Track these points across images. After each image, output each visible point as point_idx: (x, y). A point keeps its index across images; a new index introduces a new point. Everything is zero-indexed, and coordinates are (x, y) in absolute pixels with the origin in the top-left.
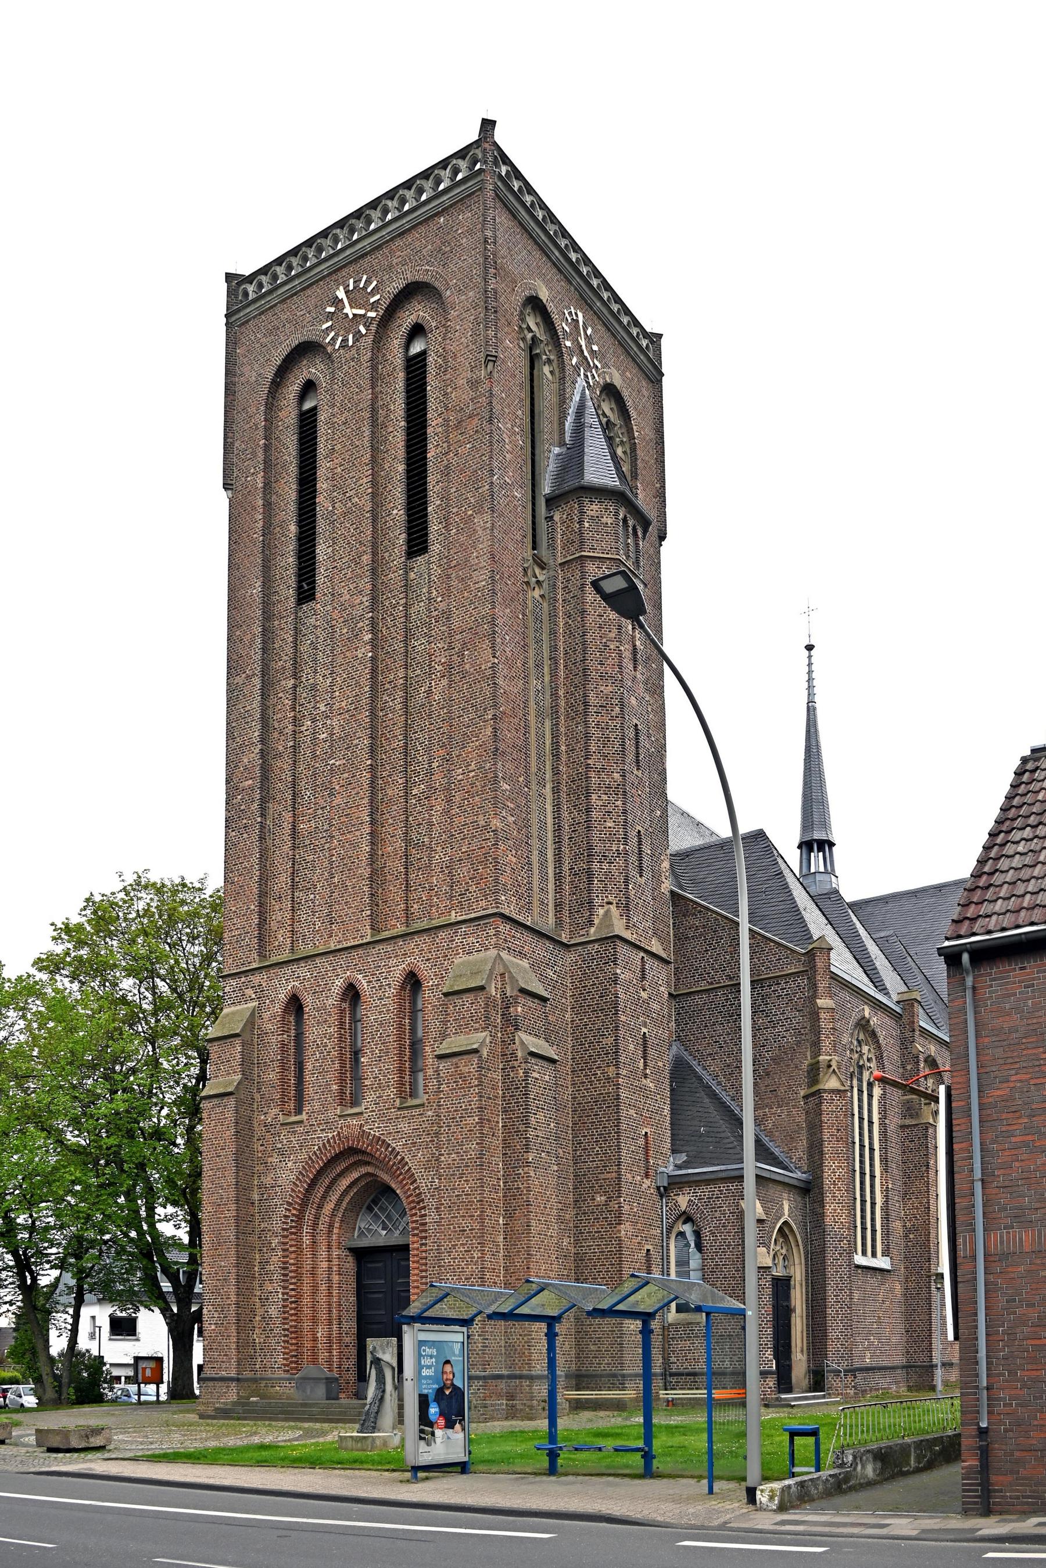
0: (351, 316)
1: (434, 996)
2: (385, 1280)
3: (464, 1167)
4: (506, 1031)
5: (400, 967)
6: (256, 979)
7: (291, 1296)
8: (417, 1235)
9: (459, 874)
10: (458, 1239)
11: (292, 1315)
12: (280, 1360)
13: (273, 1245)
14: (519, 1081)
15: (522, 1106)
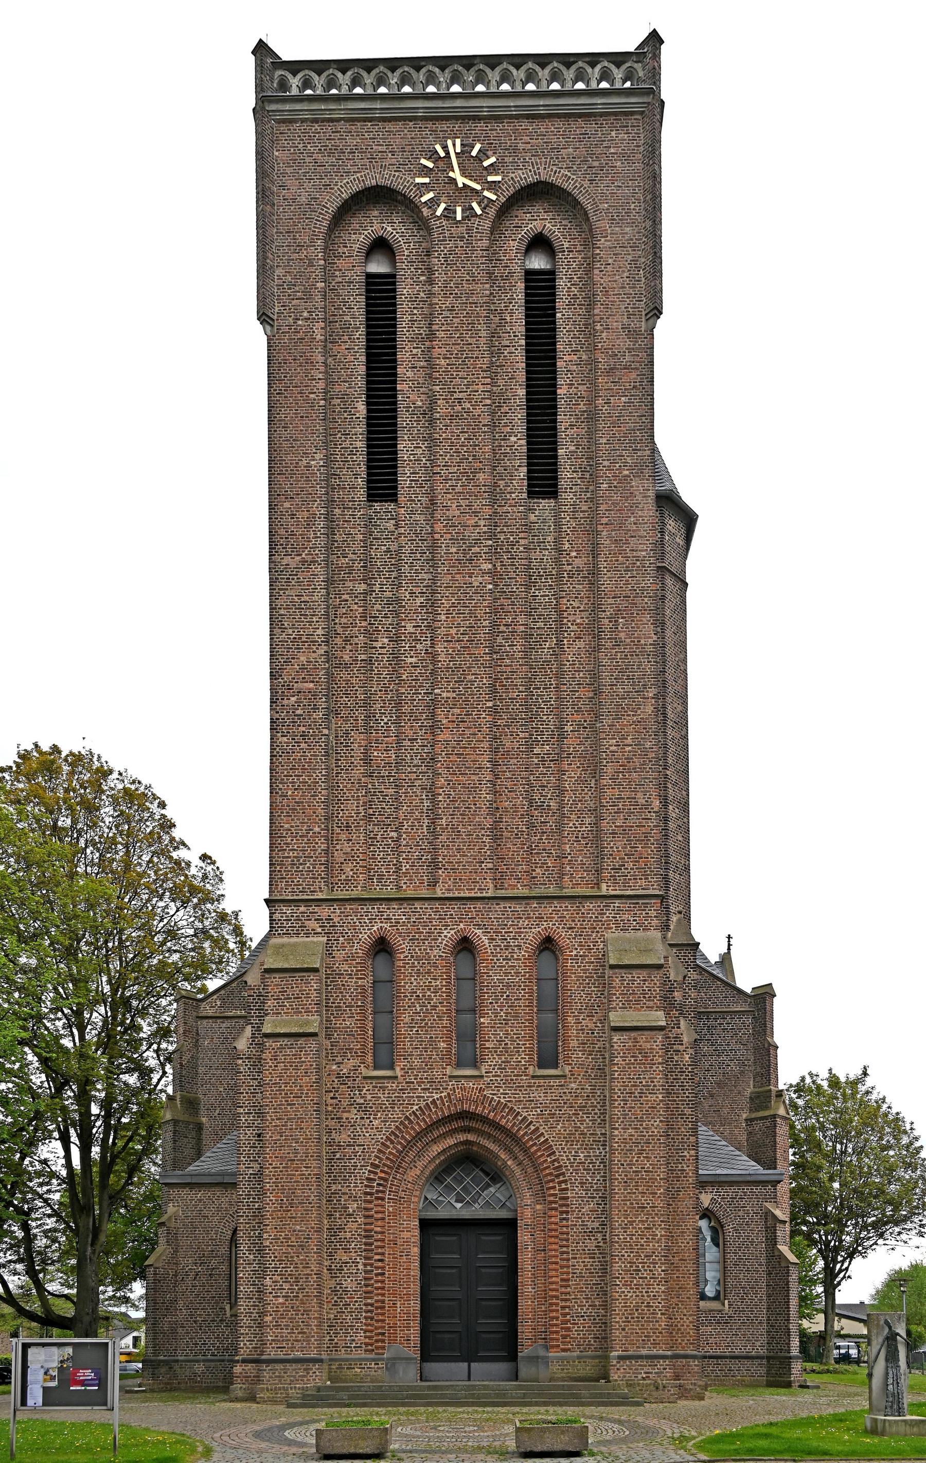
0: (460, 185)
2: (460, 1254)
3: (644, 1143)
6: (324, 911)
7: (377, 1268)
8: (556, 1209)
10: (636, 1216)
11: (377, 1288)
13: (351, 1210)
15: (687, 1090)
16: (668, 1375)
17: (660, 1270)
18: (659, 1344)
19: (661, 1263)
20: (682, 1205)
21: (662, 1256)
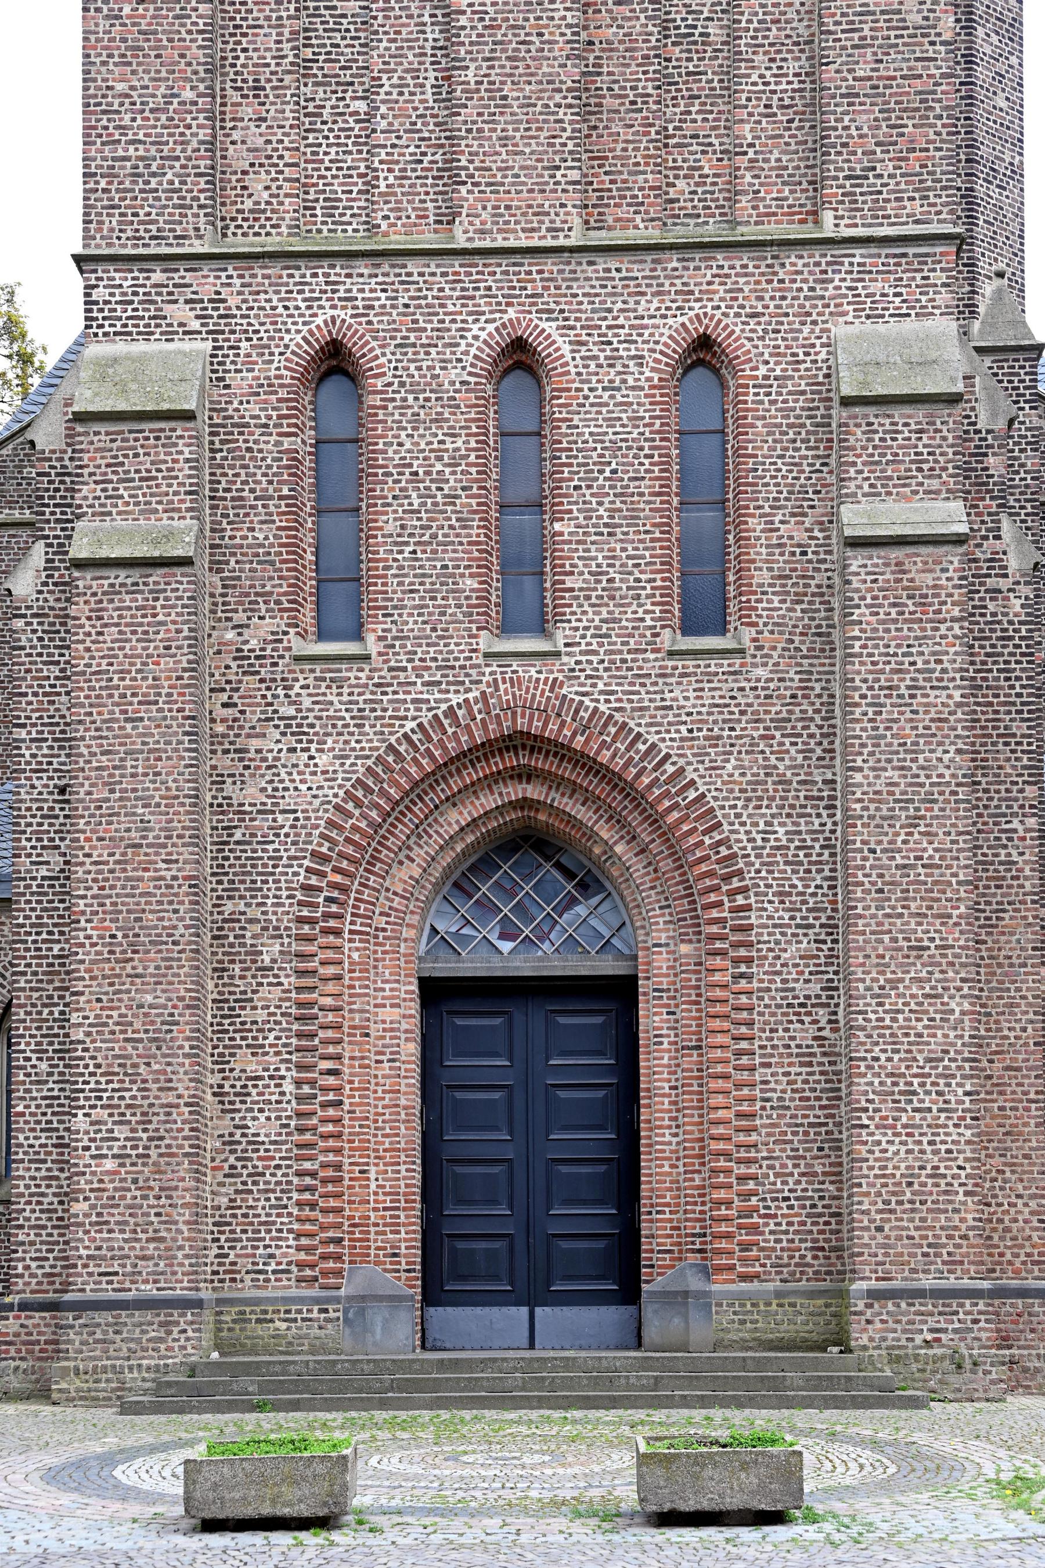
1: (773, 402)
4: (977, 506)
5: (670, 321)
9: (846, 128)
10: (905, 969)
12: (288, 1250)
13: (267, 959)
14: (1011, 623)
15: (1018, 678)
16: (984, 1335)
17: (960, 1091)
18: (962, 1263)
19: (963, 1077)
20: (1008, 942)
21: (965, 1060)
